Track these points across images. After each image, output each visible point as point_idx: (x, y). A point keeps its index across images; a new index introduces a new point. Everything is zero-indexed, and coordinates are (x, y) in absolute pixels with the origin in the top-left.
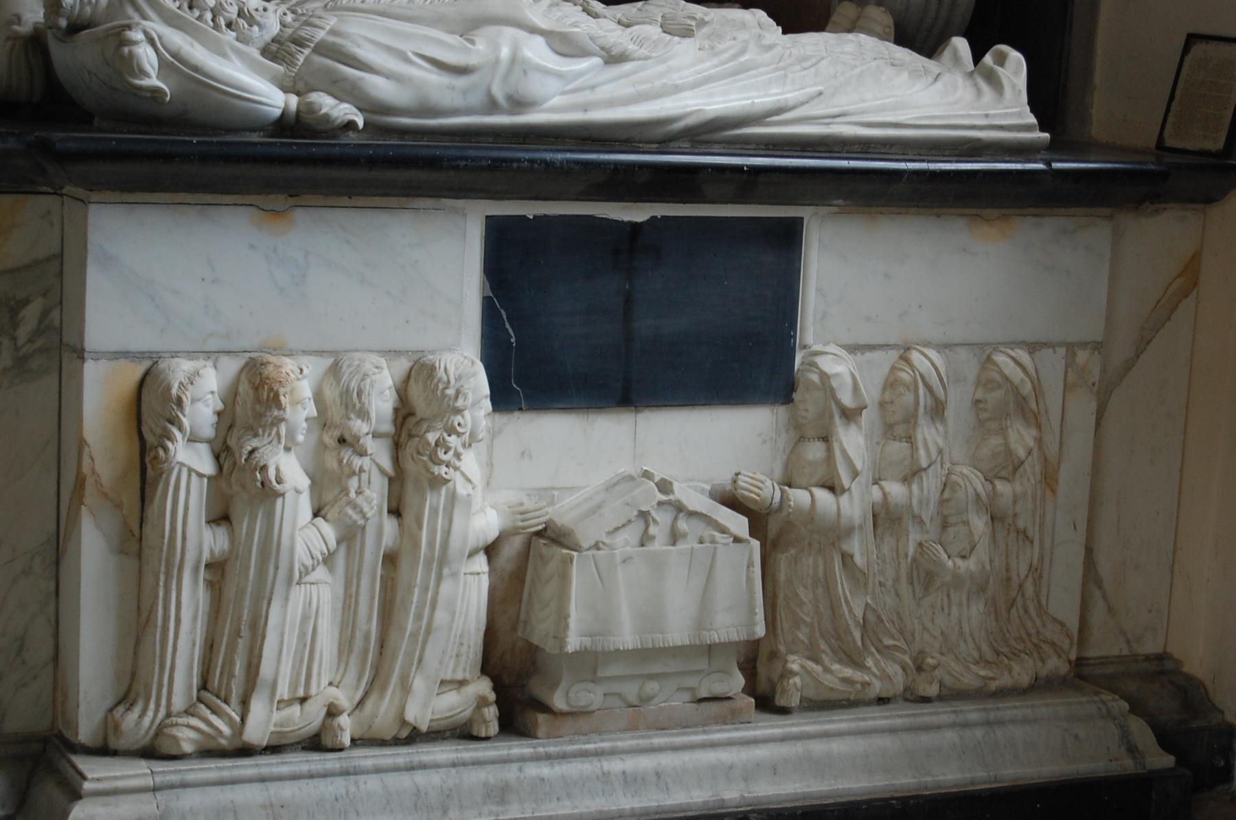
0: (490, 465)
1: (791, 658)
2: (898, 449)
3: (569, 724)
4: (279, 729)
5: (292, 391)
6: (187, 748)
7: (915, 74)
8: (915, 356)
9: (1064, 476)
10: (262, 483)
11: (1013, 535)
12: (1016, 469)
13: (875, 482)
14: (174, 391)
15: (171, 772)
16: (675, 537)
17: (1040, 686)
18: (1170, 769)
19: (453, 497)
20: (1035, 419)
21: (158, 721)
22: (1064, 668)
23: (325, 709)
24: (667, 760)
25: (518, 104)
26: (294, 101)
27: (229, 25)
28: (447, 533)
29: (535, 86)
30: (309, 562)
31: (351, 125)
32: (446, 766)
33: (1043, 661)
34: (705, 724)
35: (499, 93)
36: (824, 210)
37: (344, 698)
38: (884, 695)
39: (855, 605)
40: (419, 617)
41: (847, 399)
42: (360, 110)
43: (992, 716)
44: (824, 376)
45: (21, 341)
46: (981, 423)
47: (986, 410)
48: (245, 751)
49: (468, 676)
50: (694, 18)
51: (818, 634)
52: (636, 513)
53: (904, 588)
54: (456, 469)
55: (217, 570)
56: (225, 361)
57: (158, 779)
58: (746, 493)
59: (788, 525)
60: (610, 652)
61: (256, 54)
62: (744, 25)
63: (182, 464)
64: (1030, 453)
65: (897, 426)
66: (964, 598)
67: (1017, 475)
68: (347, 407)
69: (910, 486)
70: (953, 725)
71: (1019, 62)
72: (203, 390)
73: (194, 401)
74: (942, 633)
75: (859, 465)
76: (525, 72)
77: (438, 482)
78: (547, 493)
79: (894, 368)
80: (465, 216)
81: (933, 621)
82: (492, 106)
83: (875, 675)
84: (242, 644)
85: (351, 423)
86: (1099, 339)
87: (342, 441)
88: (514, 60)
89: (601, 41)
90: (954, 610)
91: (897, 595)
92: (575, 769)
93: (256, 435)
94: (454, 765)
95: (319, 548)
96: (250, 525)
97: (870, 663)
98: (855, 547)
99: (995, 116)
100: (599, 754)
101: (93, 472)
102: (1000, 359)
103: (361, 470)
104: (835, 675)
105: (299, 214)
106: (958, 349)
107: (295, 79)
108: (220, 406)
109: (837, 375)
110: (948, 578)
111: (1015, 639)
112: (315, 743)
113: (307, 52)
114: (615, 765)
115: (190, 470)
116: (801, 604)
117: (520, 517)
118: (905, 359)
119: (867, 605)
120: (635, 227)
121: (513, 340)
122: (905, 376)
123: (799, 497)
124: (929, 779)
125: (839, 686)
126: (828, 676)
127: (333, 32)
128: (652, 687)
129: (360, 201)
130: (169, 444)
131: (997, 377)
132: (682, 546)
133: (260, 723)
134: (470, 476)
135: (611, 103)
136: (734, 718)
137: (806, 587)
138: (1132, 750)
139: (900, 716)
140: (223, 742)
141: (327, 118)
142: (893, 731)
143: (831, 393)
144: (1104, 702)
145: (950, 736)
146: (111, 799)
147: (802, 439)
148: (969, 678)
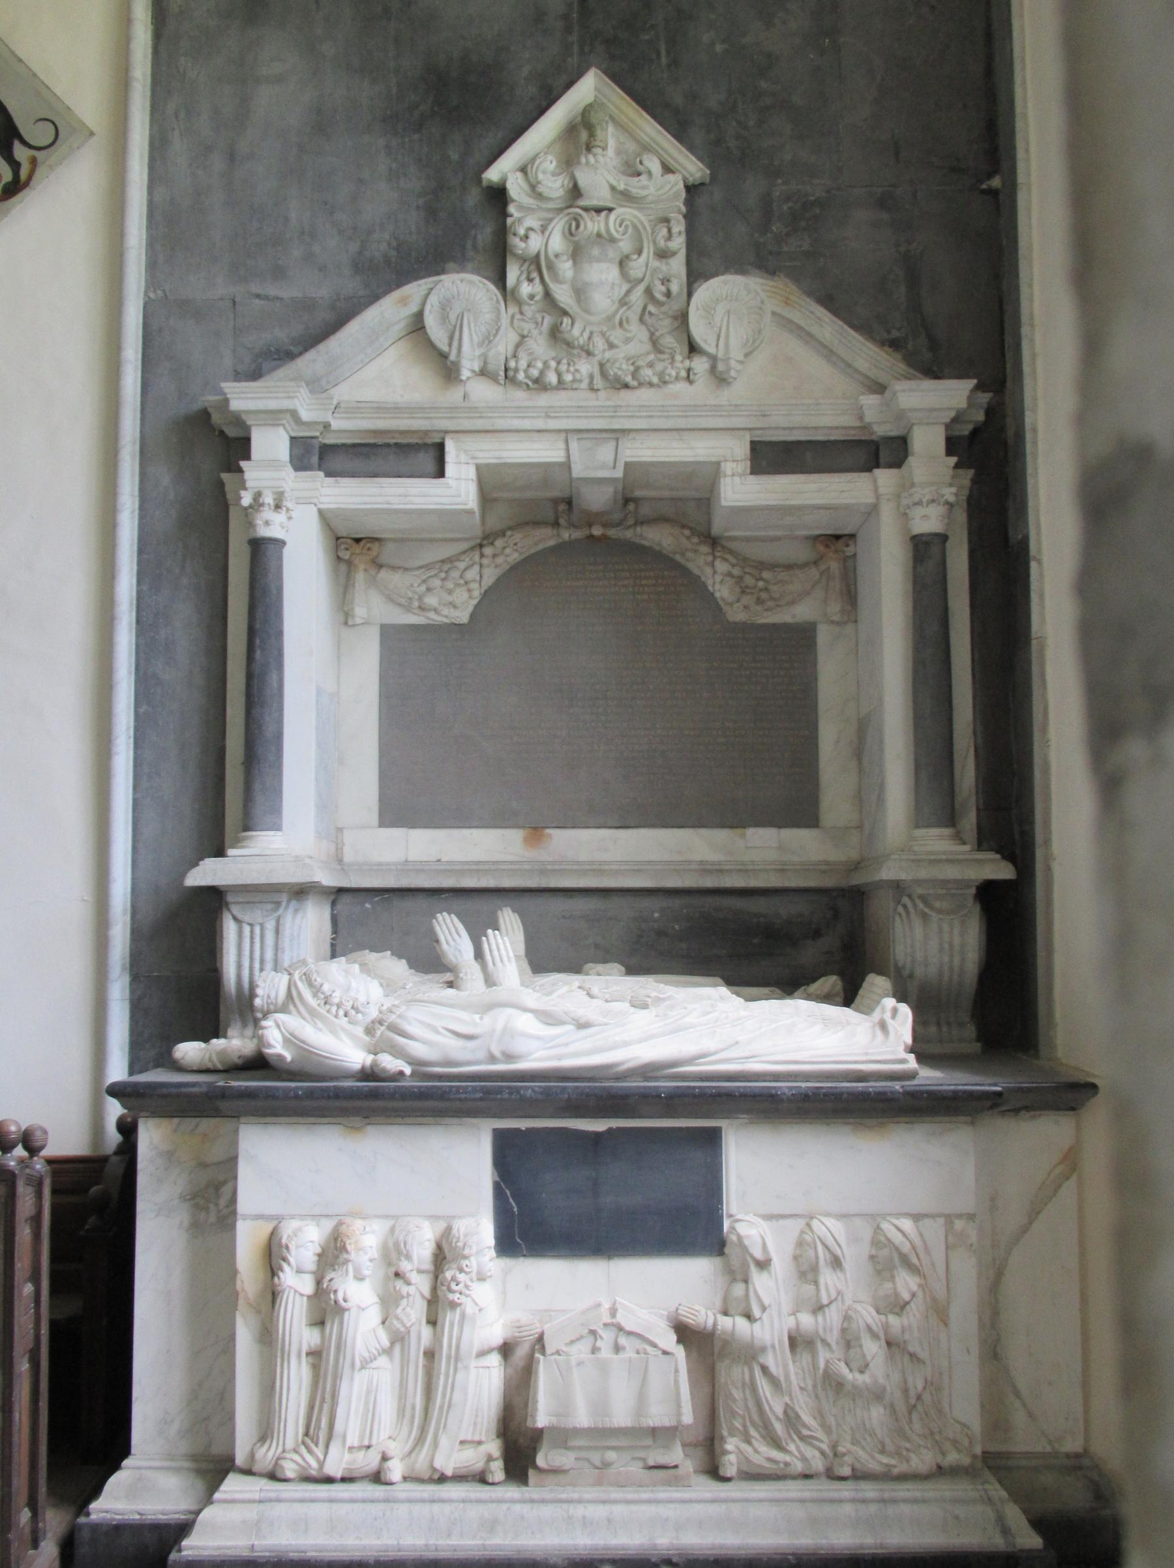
0: (504, 1293)
3: (551, 1478)
5: (356, 1242)
6: (290, 1474)
9: (954, 1312)
13: (794, 1314)
14: (284, 1241)
16: (617, 1349)
17: (940, 1472)
18: (1039, 1551)
19: (463, 1315)
20: (914, 1269)
22: (966, 1461)
23: (380, 1456)
24: (618, 1510)
25: (509, 1057)
26: (371, 1057)
29: (519, 1046)
30: (366, 1355)
31: (401, 1073)
32: (457, 1501)
33: (943, 1454)
36: (736, 1122)
37: (395, 1449)
39: (775, 1405)
41: (758, 1254)
42: (409, 1063)
43: (886, 1495)
44: (739, 1237)
45: (221, 1207)
48: (329, 1480)
49: (483, 1439)
51: (748, 1424)
53: (822, 1394)
54: (467, 1296)
55: (316, 1355)
56: (324, 1221)
57: (263, 1495)
59: (726, 1343)
61: (359, 1031)
63: (290, 1287)
64: (914, 1295)
65: (807, 1272)
70: (853, 1500)
72: (305, 1242)
73: (297, 1247)
75: (766, 1302)
77: (454, 1305)
79: (802, 1232)
82: (492, 1059)
84: (326, 1407)
87: (397, 1275)
88: (505, 1030)
92: (547, 1511)
94: (463, 1501)
95: (374, 1346)
96: (332, 1328)
97: (792, 1447)
98: (770, 1360)
100: (569, 1501)
102: (885, 1226)
103: (408, 1295)
104: (762, 1453)
105: (369, 1128)
112: (377, 1477)
113: (383, 1028)
114: (579, 1511)
115: (296, 1291)
116: (735, 1401)
118: (808, 1225)
119: (787, 1404)
120: (598, 1136)
122: (808, 1238)
123: (725, 1323)
124: (824, 1542)
125: (767, 1464)
127: (400, 1016)
128: (611, 1455)
129: (408, 1120)
131: (882, 1238)
132: (623, 1355)
135: (576, 1055)
136: (677, 1482)
138: (1006, 1531)
140: (314, 1473)
141: (384, 1070)
142: (802, 1501)
143: (744, 1249)
144: (985, 1490)
145: (848, 1508)
146: (230, 1506)
147: (734, 1280)
148: (875, 1462)
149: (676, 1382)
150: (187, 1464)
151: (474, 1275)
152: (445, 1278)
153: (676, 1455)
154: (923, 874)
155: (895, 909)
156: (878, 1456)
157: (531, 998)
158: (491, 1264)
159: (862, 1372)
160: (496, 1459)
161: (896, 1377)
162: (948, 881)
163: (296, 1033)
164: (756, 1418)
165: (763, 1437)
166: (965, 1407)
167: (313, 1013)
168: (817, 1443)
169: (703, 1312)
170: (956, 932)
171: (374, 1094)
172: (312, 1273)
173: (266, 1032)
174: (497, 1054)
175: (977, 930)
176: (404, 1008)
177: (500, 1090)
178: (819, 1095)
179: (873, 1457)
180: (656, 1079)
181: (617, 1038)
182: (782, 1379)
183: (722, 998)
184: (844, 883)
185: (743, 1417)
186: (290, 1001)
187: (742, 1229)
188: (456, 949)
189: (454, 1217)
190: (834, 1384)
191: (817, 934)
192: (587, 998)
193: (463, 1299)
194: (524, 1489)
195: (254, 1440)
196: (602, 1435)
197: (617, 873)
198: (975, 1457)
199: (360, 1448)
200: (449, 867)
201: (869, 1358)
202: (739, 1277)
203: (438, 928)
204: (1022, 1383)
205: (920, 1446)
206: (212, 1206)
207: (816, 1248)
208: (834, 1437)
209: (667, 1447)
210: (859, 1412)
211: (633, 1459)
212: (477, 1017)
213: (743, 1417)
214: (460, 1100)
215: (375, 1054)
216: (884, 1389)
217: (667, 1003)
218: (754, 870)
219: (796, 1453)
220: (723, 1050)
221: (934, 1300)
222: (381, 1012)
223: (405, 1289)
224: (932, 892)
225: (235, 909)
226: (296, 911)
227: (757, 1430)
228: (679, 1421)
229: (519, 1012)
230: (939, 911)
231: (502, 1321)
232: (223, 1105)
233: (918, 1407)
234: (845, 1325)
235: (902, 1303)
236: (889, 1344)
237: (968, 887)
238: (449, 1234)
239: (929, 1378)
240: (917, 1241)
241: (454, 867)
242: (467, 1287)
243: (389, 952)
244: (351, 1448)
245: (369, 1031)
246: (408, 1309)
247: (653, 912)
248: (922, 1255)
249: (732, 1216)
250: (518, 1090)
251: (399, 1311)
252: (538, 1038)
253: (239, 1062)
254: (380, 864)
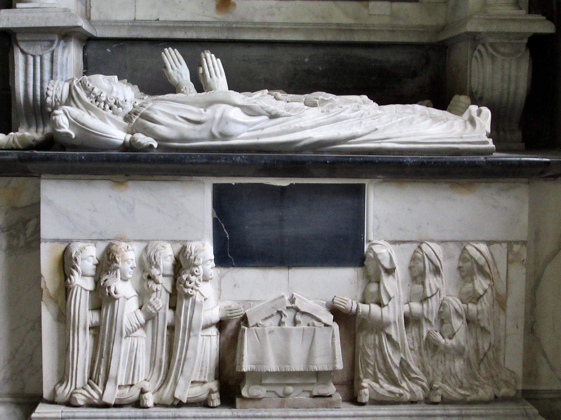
0: (220, 290)
1: (365, 380)
2: (418, 288)
3: (250, 403)
4: (118, 397)
5: (122, 256)
6: (81, 403)
7: (435, 119)
8: (424, 246)
9: (510, 302)
10: (109, 294)
13: (408, 303)
14: (73, 255)
15: (70, 412)
16: (295, 322)
17: (496, 400)
19: (194, 302)
20: (486, 275)
21: (71, 391)
22: (512, 393)
23: (139, 390)
25: (225, 136)
26: (129, 137)
27: (110, 108)
28: (191, 318)
29: (232, 129)
30: (130, 328)
31: (151, 146)
34: (317, 407)
35: (215, 132)
37: (148, 386)
39: (395, 359)
40: (181, 353)
41: (387, 265)
42: (156, 140)
43: (464, 412)
44: (375, 255)
45: (28, 236)
46: (463, 277)
48: (106, 406)
49: (207, 380)
50: (318, 99)
51: (377, 370)
52: (276, 311)
53: (424, 352)
54: (197, 290)
55: (96, 329)
56: (99, 243)
57: (64, 415)
58: (338, 305)
59: (364, 321)
60: (264, 372)
61: (120, 119)
62: (350, 102)
63: (78, 285)
64: (485, 291)
65: (417, 276)
66: (452, 357)
68: (150, 264)
69: (423, 305)
71: (488, 112)
74: (443, 373)
75: (392, 295)
76: (227, 123)
77: (188, 296)
78: (247, 303)
79: (415, 252)
80: (204, 183)
82: (213, 137)
83: (407, 391)
85: (152, 270)
86: (525, 239)
87: (149, 278)
88: (222, 118)
89: (266, 109)
93: (108, 274)
95: (135, 322)
96: (107, 312)
97: (404, 385)
99: (466, 138)
101: (46, 288)
102: (469, 248)
103: (157, 290)
104: (385, 388)
105: (130, 183)
106: (449, 243)
107: (132, 128)
108: (97, 262)
111: (484, 378)
112: (138, 404)
113: (137, 117)
115: (82, 288)
116: (369, 356)
117: (229, 312)
118: (420, 247)
120: (283, 188)
121: (228, 236)
122: (419, 255)
123: (364, 308)
125: (387, 395)
126: (382, 389)
127: (149, 109)
128: (290, 389)
129: (157, 178)
130: (72, 277)
131: (467, 256)
132: (298, 327)
133: (110, 396)
134: (203, 294)
135: (269, 135)
137: (370, 349)
139: (414, 410)
140: (96, 401)
141: (139, 144)
143: (378, 262)
147: (370, 282)
148: (455, 393)
149: (333, 344)
150: (8, 399)
151: (201, 277)
152: (183, 279)
153: (331, 389)
154: (494, 28)
155: (472, 55)
156: (459, 390)
157: (238, 97)
158: (212, 271)
159: (450, 338)
160: (216, 392)
161: (472, 342)
162: (508, 34)
163: (79, 118)
164: (382, 367)
165: (386, 379)
166: (513, 360)
167: (88, 108)
168: (419, 382)
169: (350, 301)
170: (513, 67)
171: (133, 160)
172: (92, 276)
173: (57, 117)
174: (216, 134)
175: (527, 67)
176: (150, 104)
177: (219, 158)
178: (431, 162)
179: (455, 390)
180: (322, 152)
181: (297, 125)
182: (399, 343)
183: (364, 103)
184: (434, 40)
185: (374, 366)
186: (71, 99)
188: (178, 72)
189: (186, 241)
190: (432, 347)
191: (414, 75)
192: (274, 100)
193: (194, 292)
194: (234, 410)
195: (55, 383)
196: (284, 376)
197: (280, 30)
198: (517, 391)
199: (126, 386)
200: (164, 24)
201: (456, 330)
202: (373, 279)
203: (165, 58)
204: (548, 349)
205: (485, 384)
206: (22, 236)
207: (424, 261)
208: (431, 378)
209: (326, 384)
210: (447, 363)
211: (303, 391)
212: (202, 110)
213: (374, 366)
214: (192, 163)
215: (132, 134)
216: (464, 349)
217: (328, 104)
218: (374, 30)
219: (406, 388)
220: (367, 134)
221: (498, 295)
222: (134, 107)
223: (155, 287)
224: (498, 41)
225: (23, 46)
226: (64, 48)
227: (382, 374)
228: (334, 368)
229: (231, 107)
230: (503, 54)
231: (218, 307)
232: (30, 166)
233: (483, 360)
234: (441, 310)
235: (478, 296)
236: (468, 321)
237: (522, 38)
238: (185, 251)
239: (492, 343)
240: (489, 258)
241: (168, 25)
242: (196, 284)
243: (126, 80)
244: (120, 387)
245: (127, 119)
246: (157, 299)
247: (305, 58)
248: (491, 266)
249: (370, 241)
250: (231, 157)
251: (151, 300)
252: (244, 124)
253: (34, 143)
254: (116, 21)
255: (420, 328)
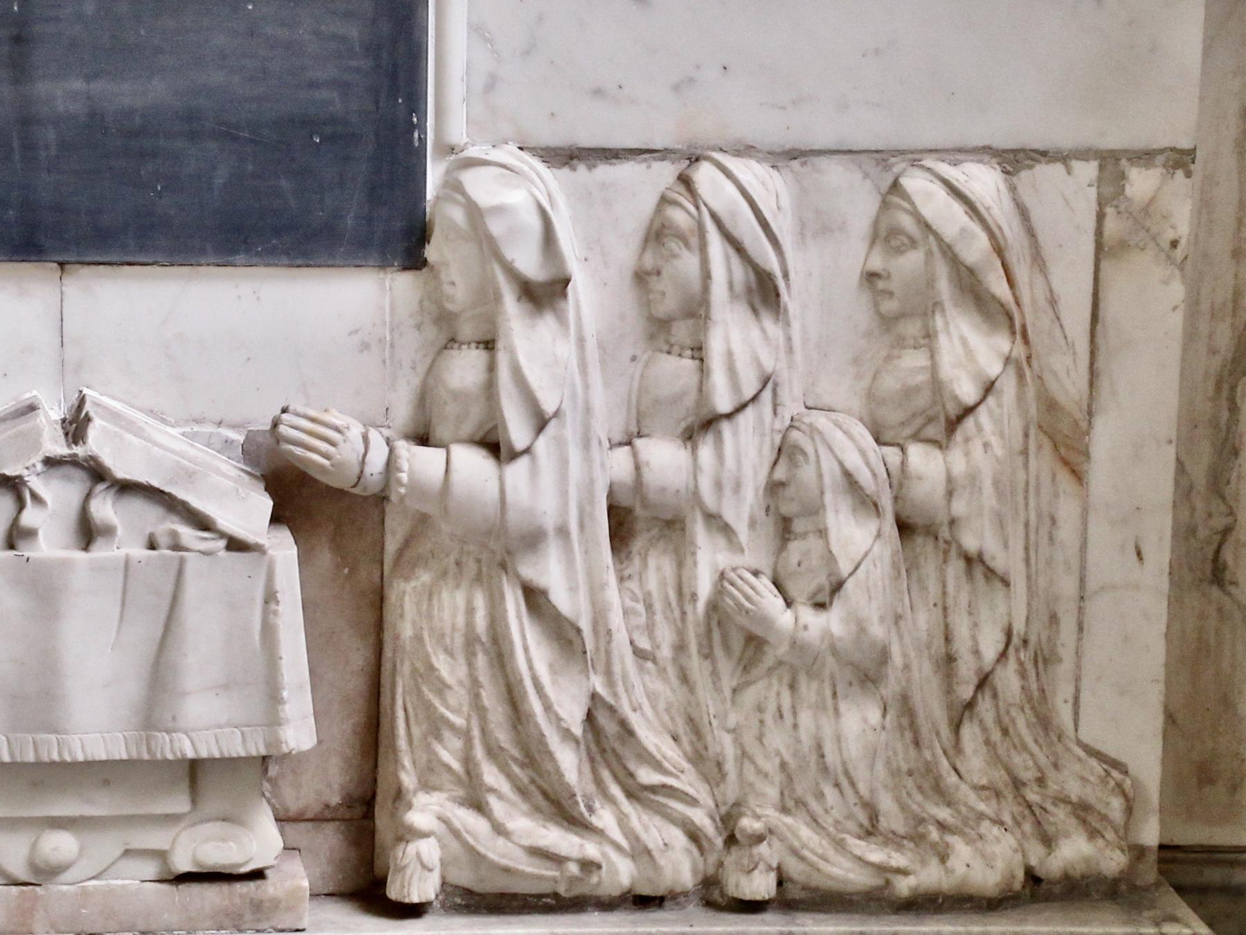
1: (421, 799)
2: (675, 371)
8: (705, 175)
11: (955, 567)
12: (953, 424)
16: (88, 532)
20: (997, 314)
22: (1113, 862)
33: (1048, 841)
38: (646, 891)
44: (475, 212)
46: (887, 322)
47: (891, 294)
58: (298, 451)
60: (46, 763)
64: (989, 388)
67: (959, 436)
74: (783, 765)
79: (664, 201)
81: (760, 738)
83: (618, 847)
86: (1185, 144)
90: (805, 718)
91: (685, 679)
97: (604, 818)
98: (550, 571)
102: (915, 183)
106: (823, 162)
109: (499, 210)
110: (782, 650)
111: (979, 788)
116: (442, 688)
118: (685, 181)
122: (679, 218)
126: (501, 841)
128: (60, 845)
132: (101, 552)
137: (449, 652)
143: (490, 248)
147: (452, 341)
187: (483, 187)
208: (731, 791)
236: (905, 528)
255: (683, 558)
